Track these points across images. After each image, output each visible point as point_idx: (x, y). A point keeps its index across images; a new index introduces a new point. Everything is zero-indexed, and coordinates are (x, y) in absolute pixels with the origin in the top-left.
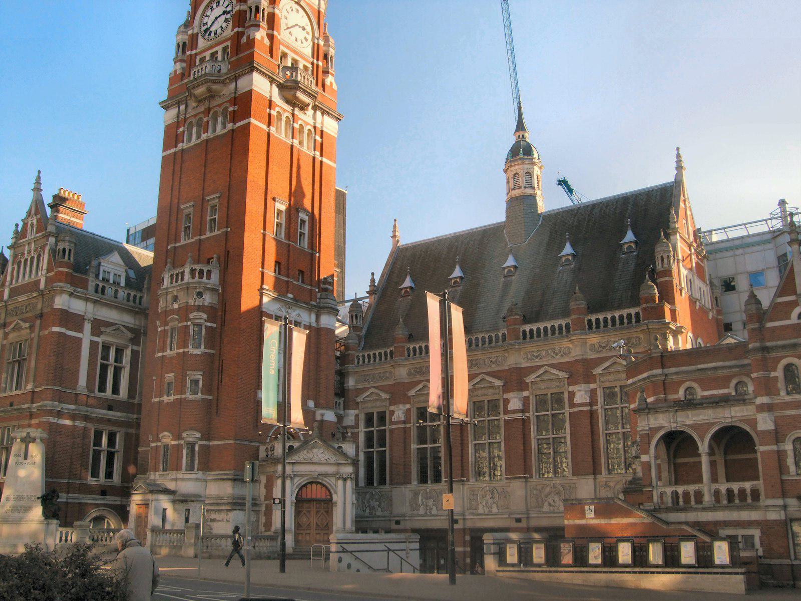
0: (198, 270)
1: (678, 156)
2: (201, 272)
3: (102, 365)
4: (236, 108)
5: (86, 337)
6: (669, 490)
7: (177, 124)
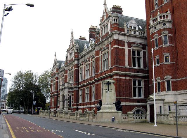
0: (162, 16)
2: (164, 16)
3: (133, 57)
5: (126, 48)
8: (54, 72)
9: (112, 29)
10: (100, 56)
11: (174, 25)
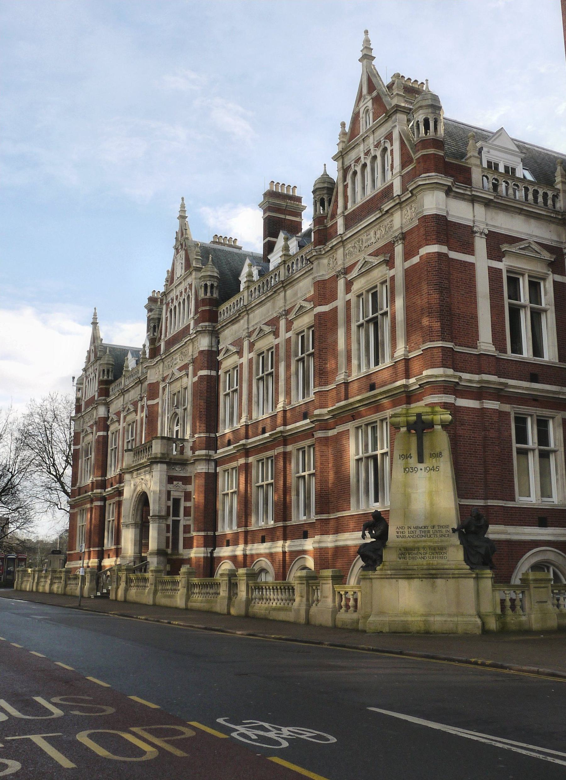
5: (481, 261)
8: (89, 396)
9: (198, 315)
10: (340, 303)
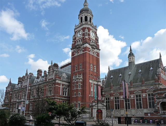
1: (160, 54)
4: (84, 49)
5: (61, 87)
6: (163, 112)
7: (74, 52)
11: (83, 80)
